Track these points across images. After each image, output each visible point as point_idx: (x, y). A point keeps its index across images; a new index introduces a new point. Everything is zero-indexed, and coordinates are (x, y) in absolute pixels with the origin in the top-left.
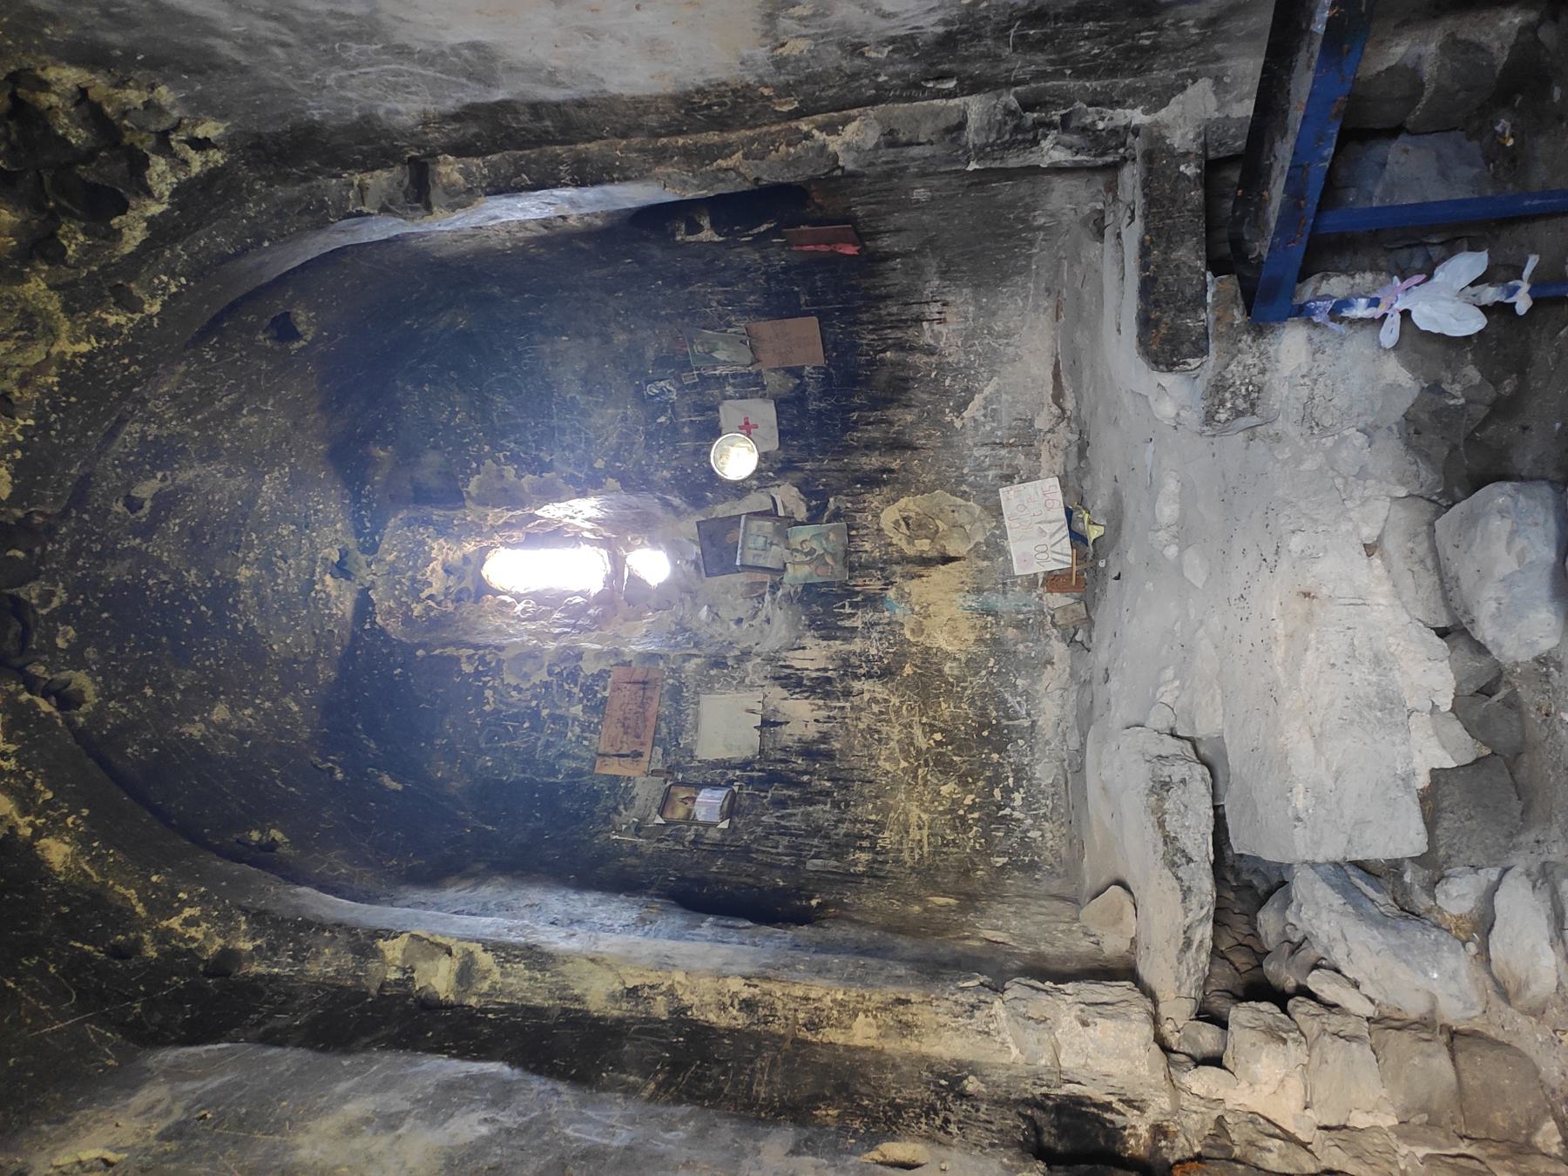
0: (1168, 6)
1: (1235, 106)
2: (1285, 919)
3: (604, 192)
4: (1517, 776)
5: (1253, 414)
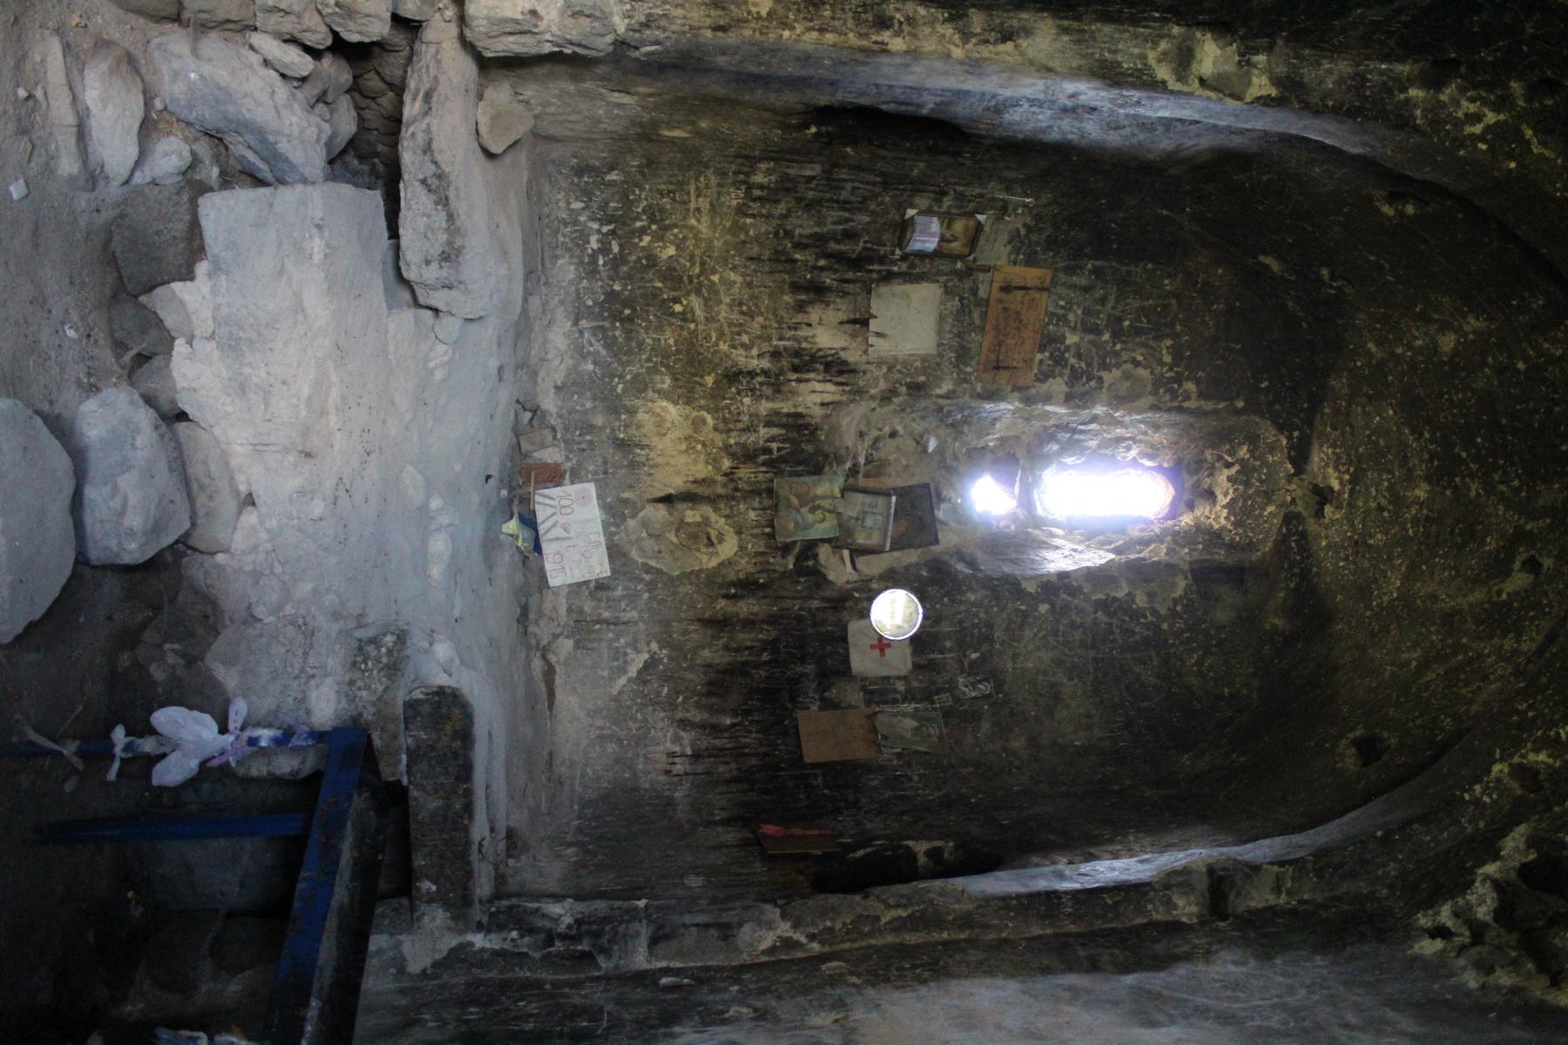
0: (452, 1040)
2: (331, 125)
3: (1024, 885)
4: (115, 275)
5: (360, 640)
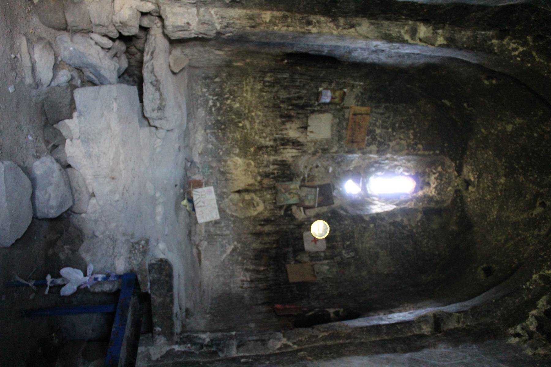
1: (144, 350)
5: (133, 243)
